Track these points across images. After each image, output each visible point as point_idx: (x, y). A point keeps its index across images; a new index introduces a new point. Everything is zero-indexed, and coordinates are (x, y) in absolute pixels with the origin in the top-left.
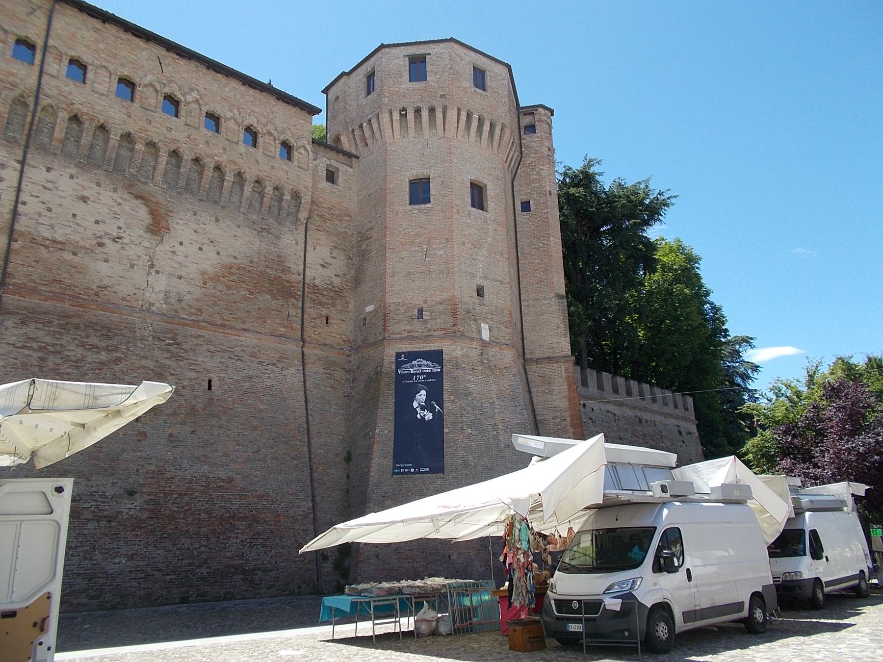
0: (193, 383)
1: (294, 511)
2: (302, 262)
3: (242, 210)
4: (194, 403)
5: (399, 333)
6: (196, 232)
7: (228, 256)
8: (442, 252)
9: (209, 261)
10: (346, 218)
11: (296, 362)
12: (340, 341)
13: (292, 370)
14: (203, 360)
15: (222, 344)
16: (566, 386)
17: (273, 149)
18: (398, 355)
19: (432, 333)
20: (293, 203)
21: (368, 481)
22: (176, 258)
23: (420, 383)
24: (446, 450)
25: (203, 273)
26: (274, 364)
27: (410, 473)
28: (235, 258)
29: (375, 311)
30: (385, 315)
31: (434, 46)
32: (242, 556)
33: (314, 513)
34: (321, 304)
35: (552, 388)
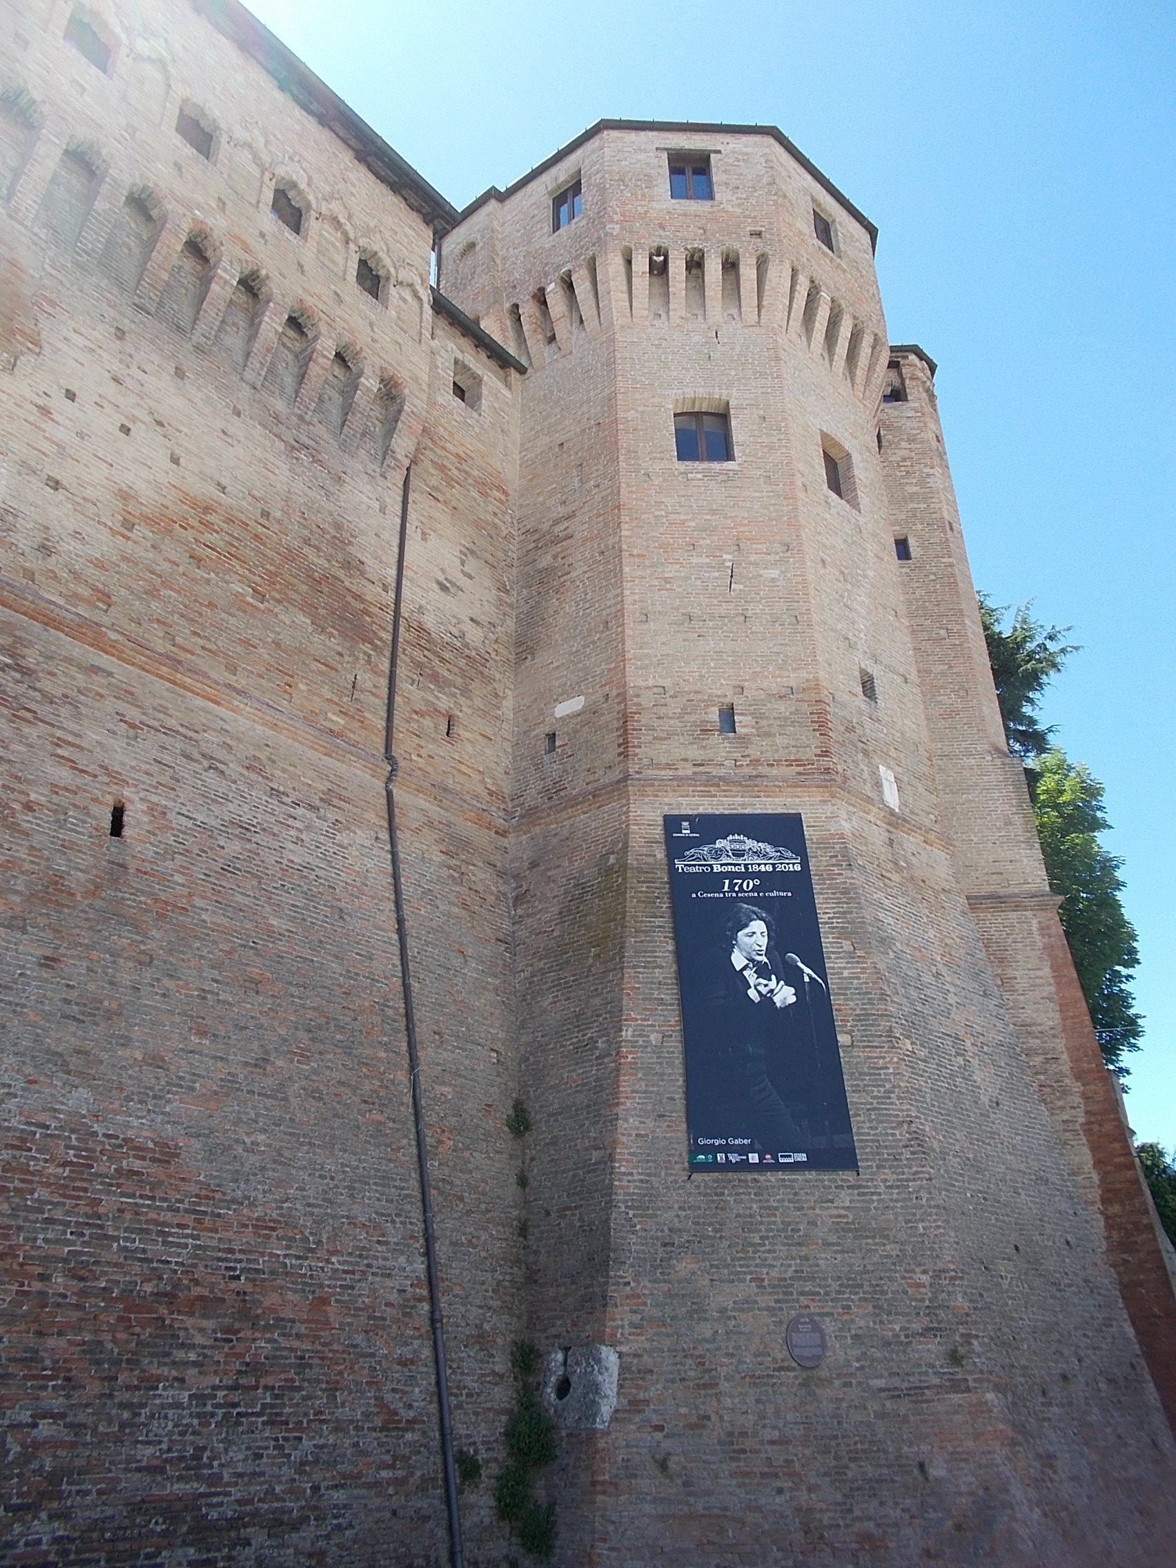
0: (65, 799)
2: (394, 560)
3: (249, 375)
4: (60, 864)
5: (668, 766)
6: (116, 380)
8: (774, 573)
9: (145, 470)
10: (498, 495)
11: (371, 816)
12: (480, 789)
13: (362, 836)
14: (99, 737)
15: (164, 710)
16: (1047, 971)
17: (339, 259)
18: (672, 823)
19: (764, 770)
20: (377, 412)
21: (609, 1190)
22: (48, 426)
23: (747, 900)
24: (851, 1098)
25: (125, 496)
26: (312, 807)
27: (745, 1166)
28: (223, 489)
29: (590, 712)
30: (625, 718)
31: (727, 138)
32: (194, 1464)
33: (433, 1300)
34: (435, 677)
35: (1010, 972)
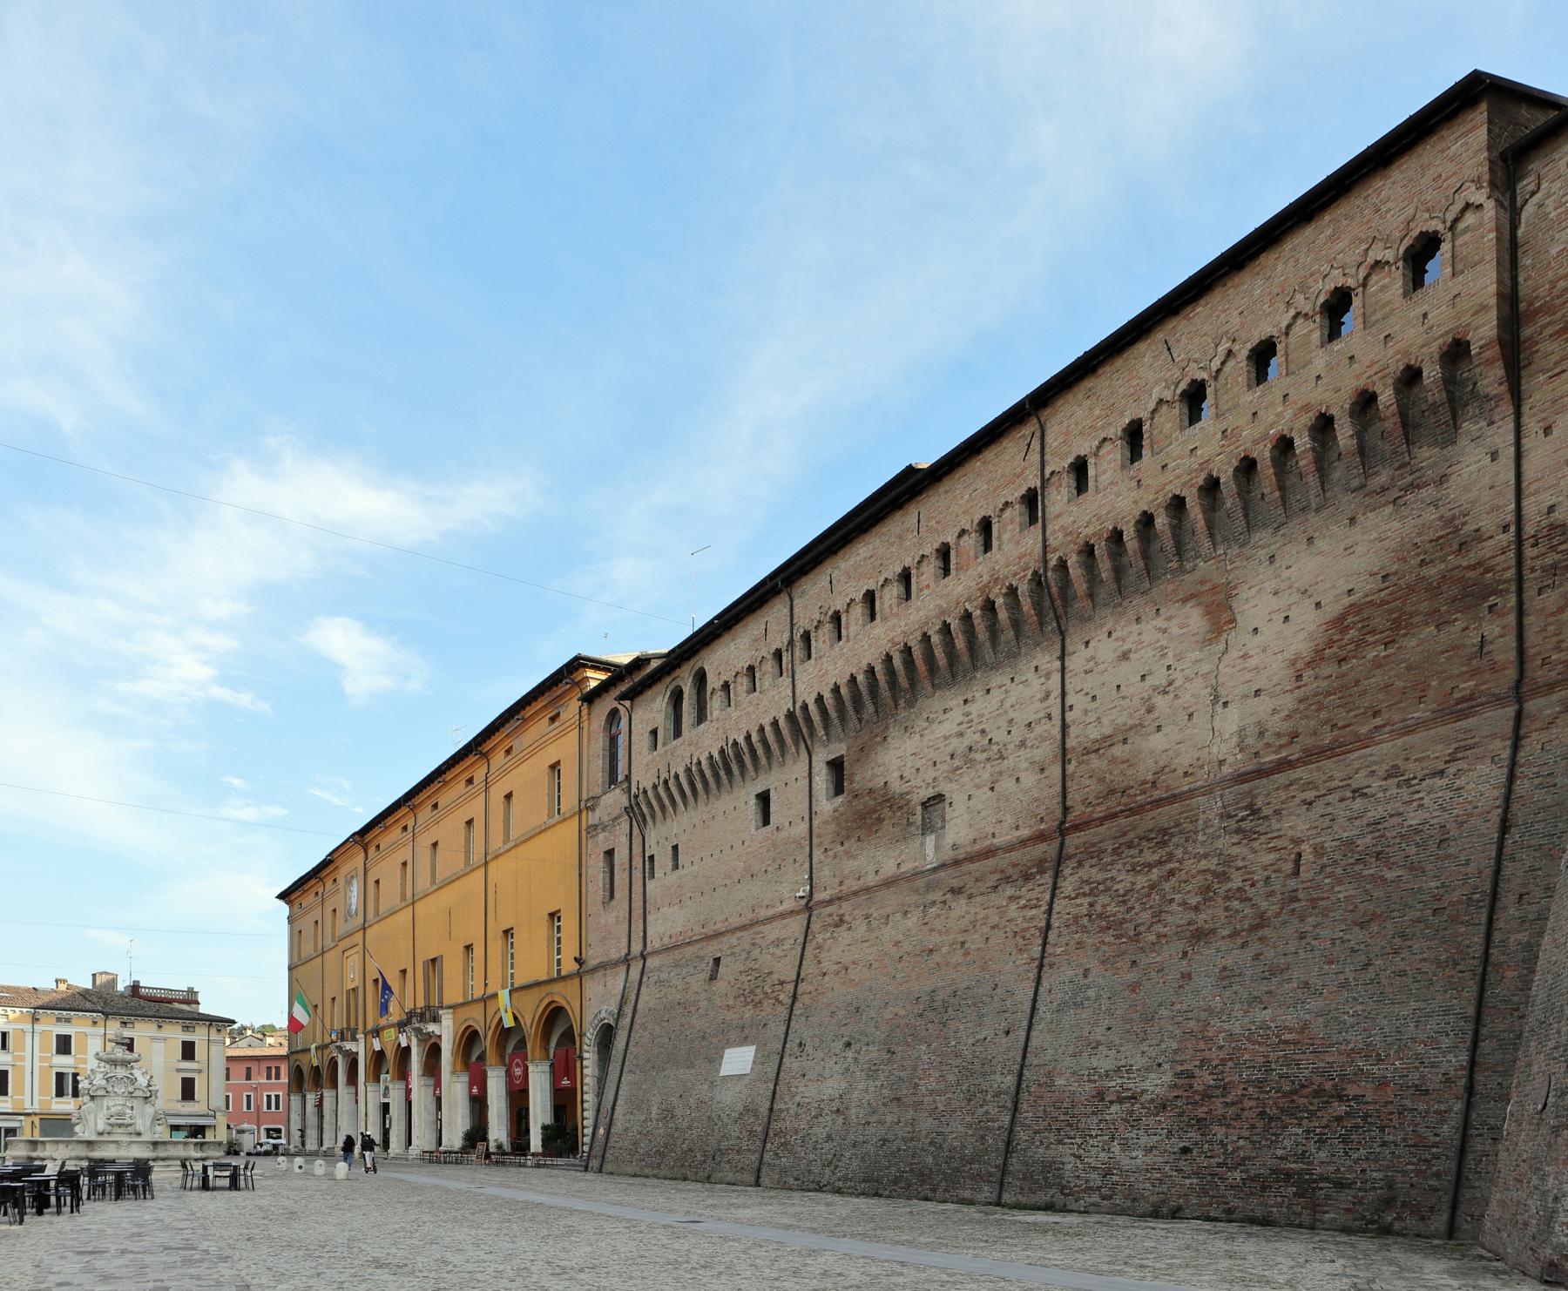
1: (1423, 1077)
7: (1337, 598)
